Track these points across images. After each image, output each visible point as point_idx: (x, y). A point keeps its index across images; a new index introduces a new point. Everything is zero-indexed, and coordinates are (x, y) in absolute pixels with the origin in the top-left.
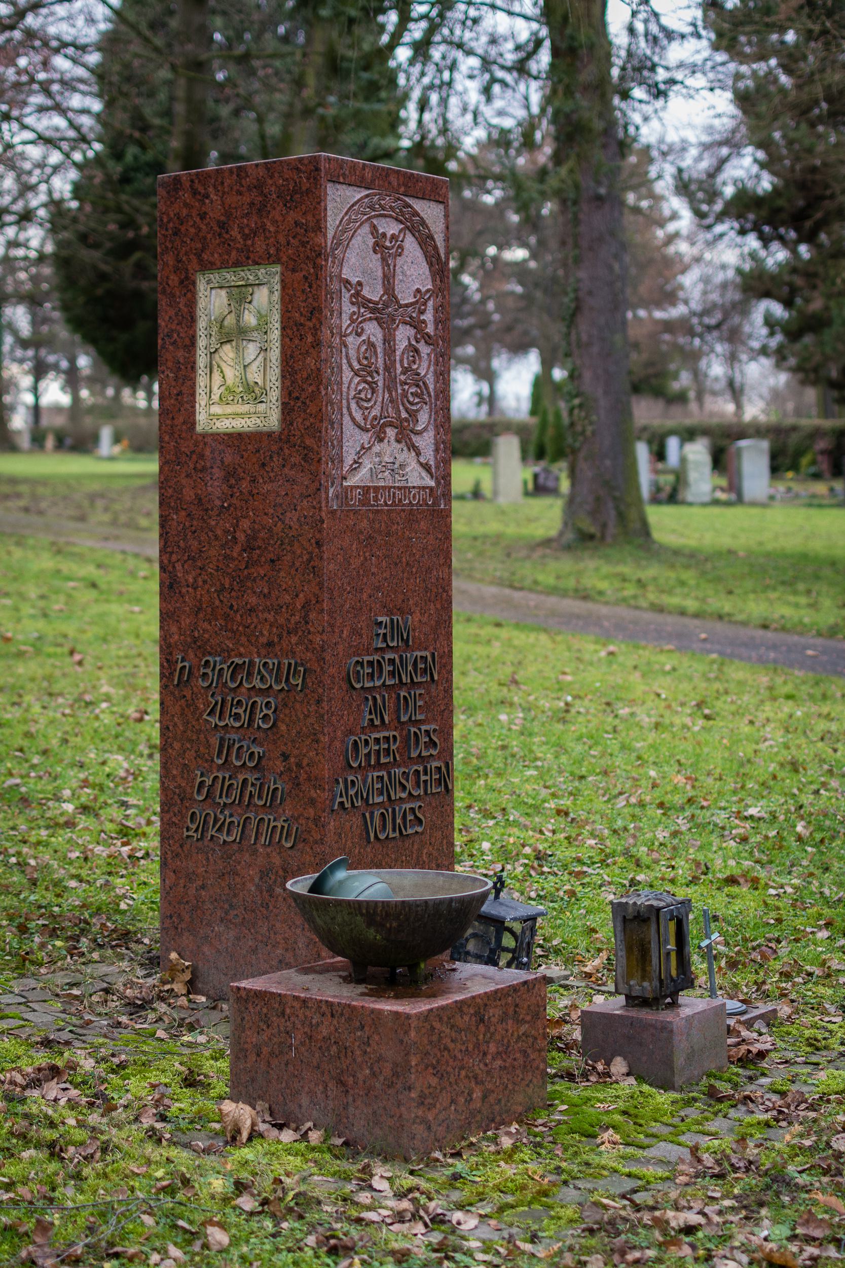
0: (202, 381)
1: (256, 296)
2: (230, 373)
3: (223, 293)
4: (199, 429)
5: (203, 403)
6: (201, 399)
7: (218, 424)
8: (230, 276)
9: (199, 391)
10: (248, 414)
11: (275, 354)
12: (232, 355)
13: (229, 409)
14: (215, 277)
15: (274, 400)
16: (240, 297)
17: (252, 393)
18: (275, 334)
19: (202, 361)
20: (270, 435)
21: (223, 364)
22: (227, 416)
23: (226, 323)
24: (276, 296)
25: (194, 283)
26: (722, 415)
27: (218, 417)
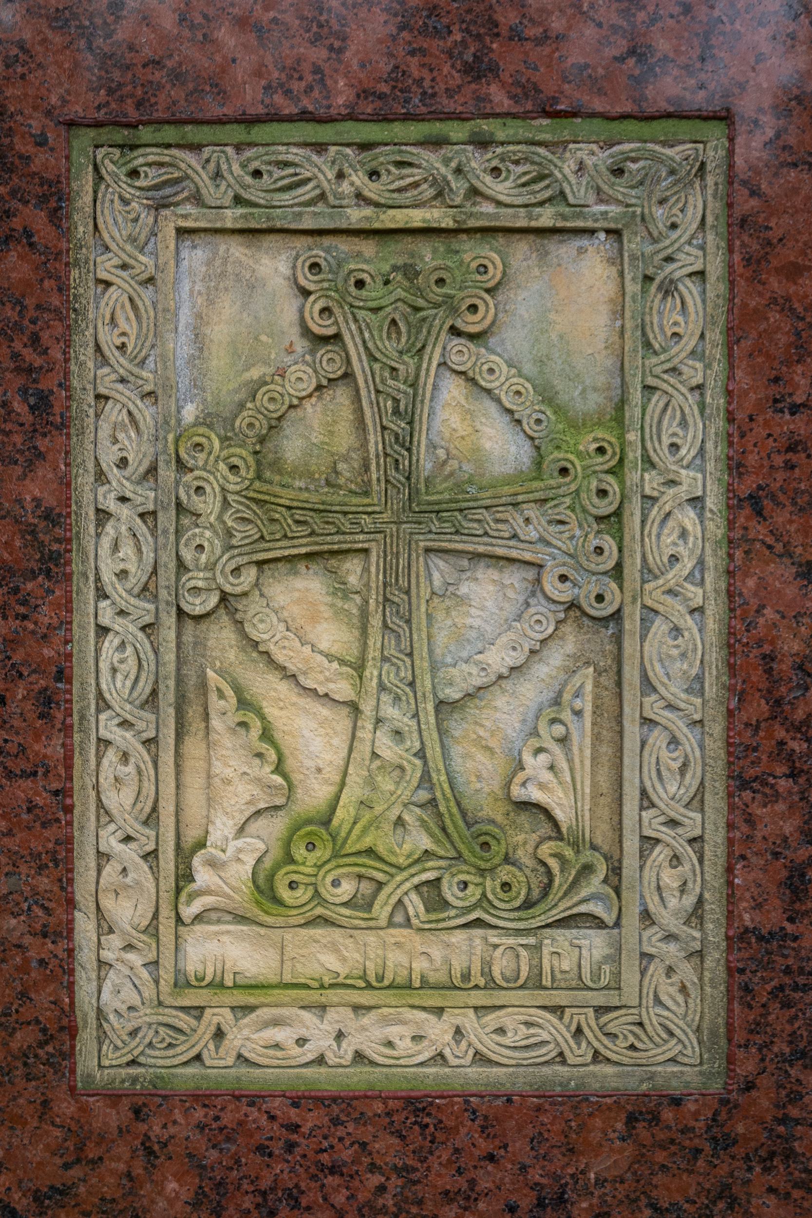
0: (113, 782)
1: (524, 302)
2: (315, 741)
3: (274, 266)
4: (97, 1061)
5: (127, 912)
6: (115, 893)
7: (248, 1037)
8: (334, 176)
9: (93, 837)
10: (479, 987)
11: (682, 650)
12: (333, 635)
13: (325, 955)
14: (217, 171)
15: (671, 911)
16: (408, 301)
17: (489, 856)
18: (684, 533)
19: (112, 663)
20: (642, 1112)
21: (269, 689)
22: (315, 994)
23: (292, 447)
24: (692, 319)
25: (55, 198)
26: (478, 455)
27: (248, 995)
